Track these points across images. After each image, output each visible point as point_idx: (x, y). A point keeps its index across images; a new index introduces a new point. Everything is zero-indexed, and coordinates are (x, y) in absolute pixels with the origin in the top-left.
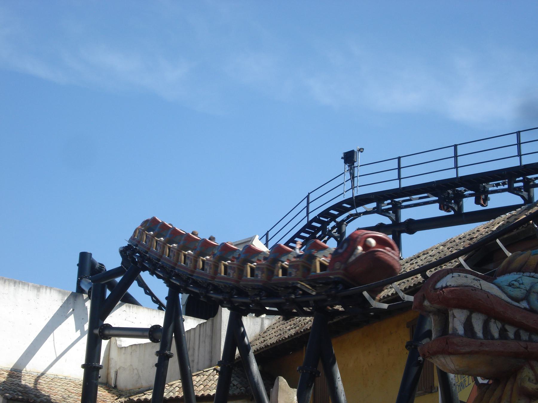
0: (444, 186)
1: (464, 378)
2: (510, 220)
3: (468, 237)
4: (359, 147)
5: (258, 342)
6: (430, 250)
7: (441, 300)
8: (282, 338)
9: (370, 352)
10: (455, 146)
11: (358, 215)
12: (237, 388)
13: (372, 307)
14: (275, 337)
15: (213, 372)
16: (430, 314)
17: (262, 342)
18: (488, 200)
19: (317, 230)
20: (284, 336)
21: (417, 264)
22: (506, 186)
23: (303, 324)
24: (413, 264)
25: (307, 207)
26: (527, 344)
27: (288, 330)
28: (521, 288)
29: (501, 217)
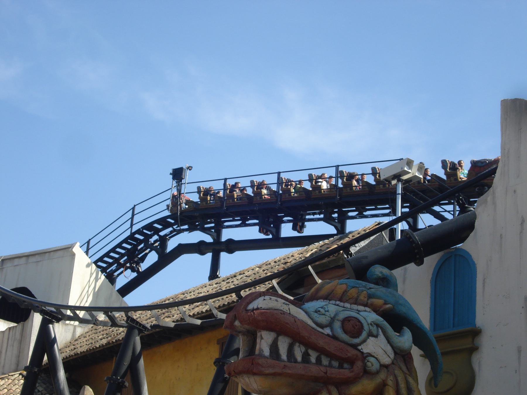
2: (323, 248)
3: (283, 261)
5: (68, 350)
6: (246, 270)
8: (93, 347)
9: (179, 366)
13: (186, 322)
14: (86, 346)
15: (18, 376)
16: (239, 334)
17: (73, 349)
19: (140, 242)
20: (95, 345)
23: (116, 334)
24: (229, 283)
25: (132, 218)
26: (326, 369)
27: (100, 340)
29: (315, 245)
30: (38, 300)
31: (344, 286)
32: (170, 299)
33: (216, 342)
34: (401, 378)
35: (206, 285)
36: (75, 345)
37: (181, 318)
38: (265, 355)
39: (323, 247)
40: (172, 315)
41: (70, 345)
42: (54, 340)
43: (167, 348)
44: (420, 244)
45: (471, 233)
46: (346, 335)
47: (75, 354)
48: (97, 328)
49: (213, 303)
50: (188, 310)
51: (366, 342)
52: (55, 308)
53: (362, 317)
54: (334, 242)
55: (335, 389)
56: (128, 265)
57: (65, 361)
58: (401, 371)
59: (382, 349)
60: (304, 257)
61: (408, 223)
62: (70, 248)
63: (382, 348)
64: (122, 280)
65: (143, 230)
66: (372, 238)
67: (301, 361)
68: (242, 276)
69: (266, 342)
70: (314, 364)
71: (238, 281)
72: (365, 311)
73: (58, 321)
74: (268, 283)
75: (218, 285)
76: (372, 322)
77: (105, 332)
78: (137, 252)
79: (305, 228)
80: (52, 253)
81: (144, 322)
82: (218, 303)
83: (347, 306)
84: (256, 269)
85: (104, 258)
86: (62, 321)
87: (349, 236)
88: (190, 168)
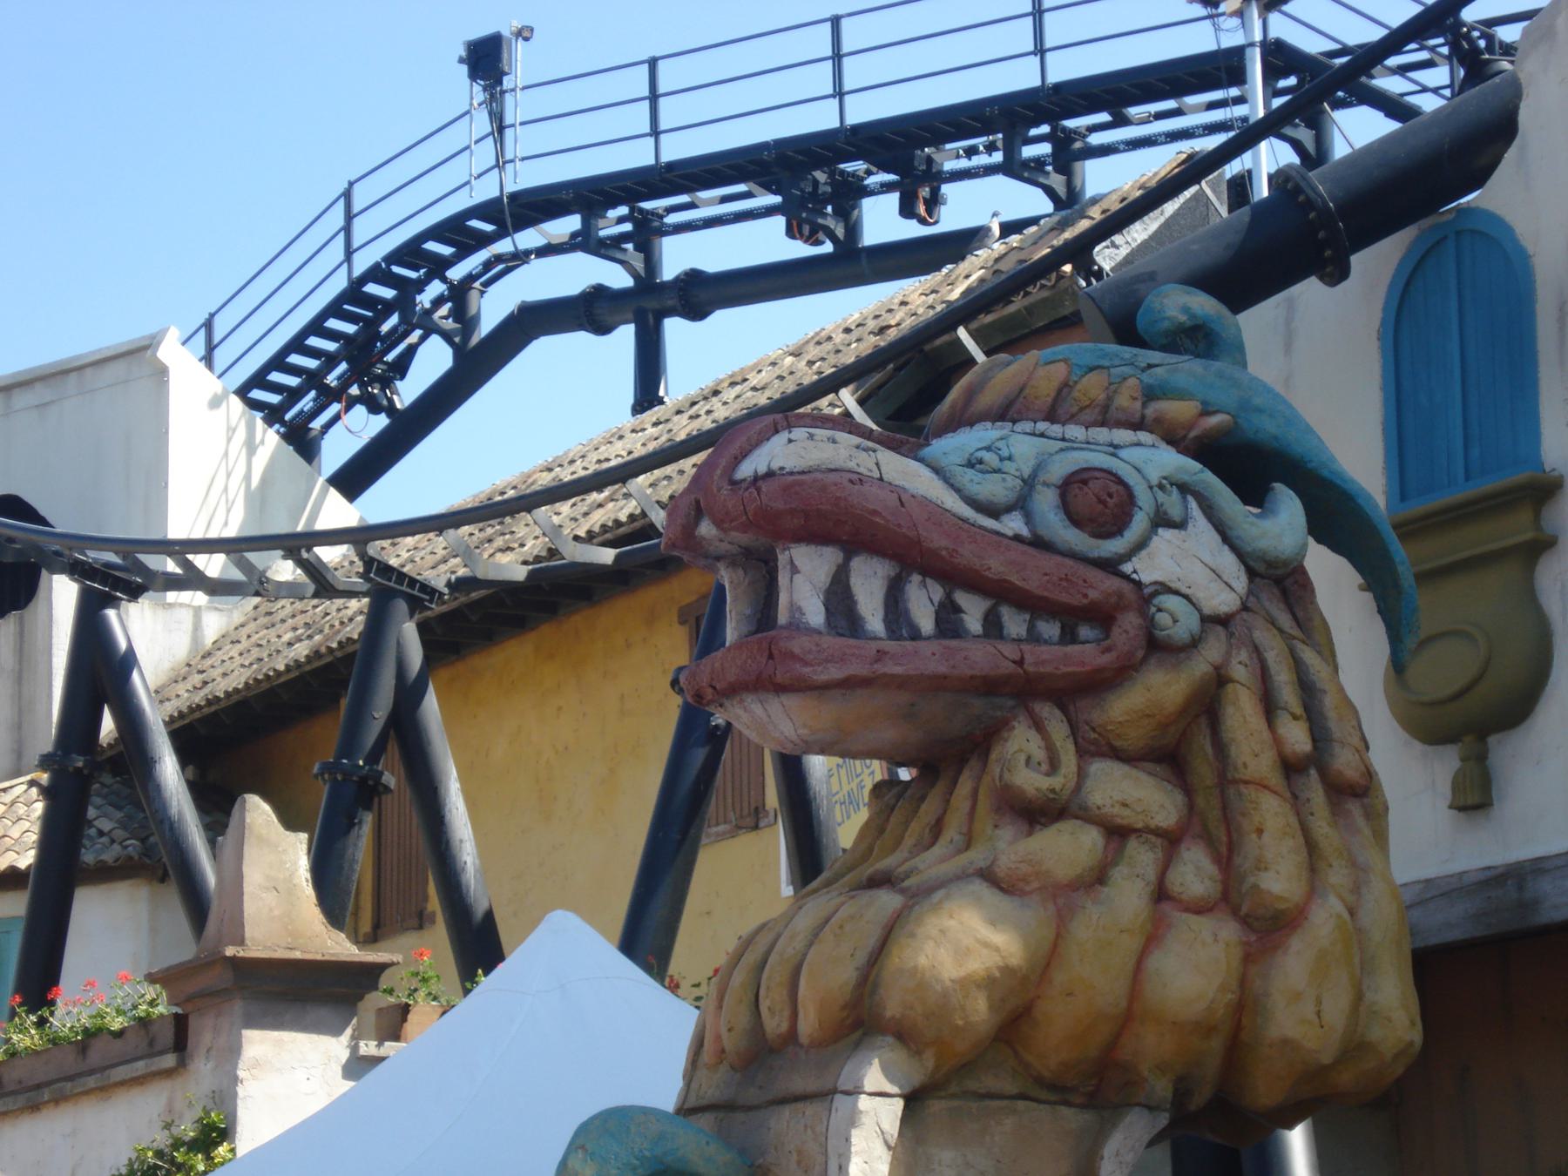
0: (800, 157)
1: (859, 779)
2: (1003, 266)
3: (872, 324)
4: (517, 24)
5: (181, 689)
6: (752, 369)
7: (751, 518)
8: (264, 670)
9: (560, 709)
10: (836, 21)
11: (519, 258)
12: (113, 841)
13: (564, 559)
14: (242, 670)
15: (26, 791)
16: (718, 564)
17: (198, 686)
18: (940, 204)
19: (384, 308)
20: (272, 665)
21: (711, 418)
22: (998, 157)
23: (337, 623)
24: (698, 416)
25: (347, 229)
26: (1021, 650)
27: (285, 646)
28: (1004, 473)
29: (977, 256)
30: (58, 530)
31: (1060, 371)
32: (507, 490)
33: (675, 619)
34: (1275, 652)
35: (621, 433)
36: (204, 671)
37: (550, 550)
38: (809, 624)
39: (1007, 258)
40: (519, 542)
41: (189, 673)
42: (128, 661)
43: (515, 653)
44: (1333, 209)
45: (1505, 151)
46: (1077, 531)
47: (208, 700)
48: (274, 607)
49: (649, 491)
50: (568, 519)
51: (1148, 546)
52: (116, 553)
53: (1129, 467)
54: (1041, 237)
55: (1057, 712)
56: (354, 390)
57: (176, 725)
58: (1275, 631)
59: (1206, 565)
60: (943, 302)
61: (1297, 146)
62: (145, 348)
63: (1202, 562)
64: (340, 446)
65: (388, 266)
66: (1170, 208)
67: (932, 632)
68: (738, 388)
69: (811, 583)
70: (978, 636)
71: (727, 409)
72: (1138, 444)
73: (135, 592)
74: (830, 405)
75: (660, 427)
76: (1165, 478)
77: (300, 620)
78: (379, 344)
79: (944, 204)
80: (89, 371)
81: (427, 573)
82: (665, 486)
83: (1075, 435)
84: (783, 360)
85: (270, 373)
86: (146, 594)
87: (1091, 214)
88: (526, 34)
